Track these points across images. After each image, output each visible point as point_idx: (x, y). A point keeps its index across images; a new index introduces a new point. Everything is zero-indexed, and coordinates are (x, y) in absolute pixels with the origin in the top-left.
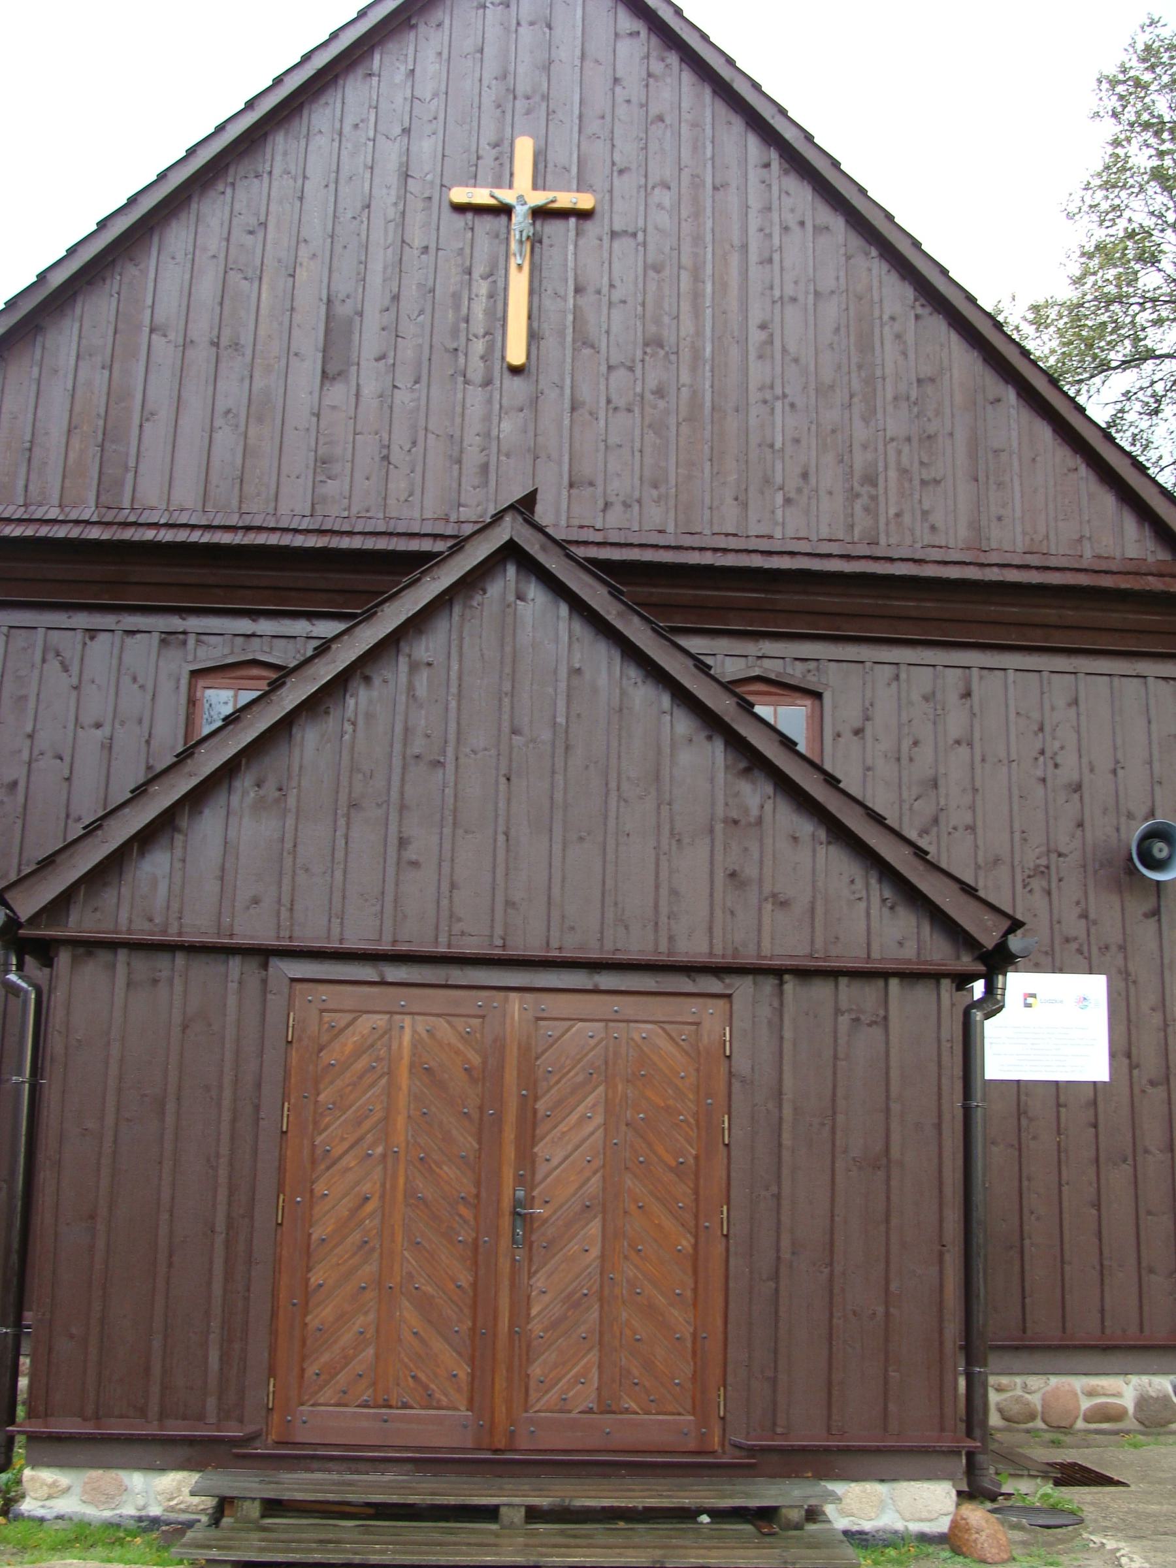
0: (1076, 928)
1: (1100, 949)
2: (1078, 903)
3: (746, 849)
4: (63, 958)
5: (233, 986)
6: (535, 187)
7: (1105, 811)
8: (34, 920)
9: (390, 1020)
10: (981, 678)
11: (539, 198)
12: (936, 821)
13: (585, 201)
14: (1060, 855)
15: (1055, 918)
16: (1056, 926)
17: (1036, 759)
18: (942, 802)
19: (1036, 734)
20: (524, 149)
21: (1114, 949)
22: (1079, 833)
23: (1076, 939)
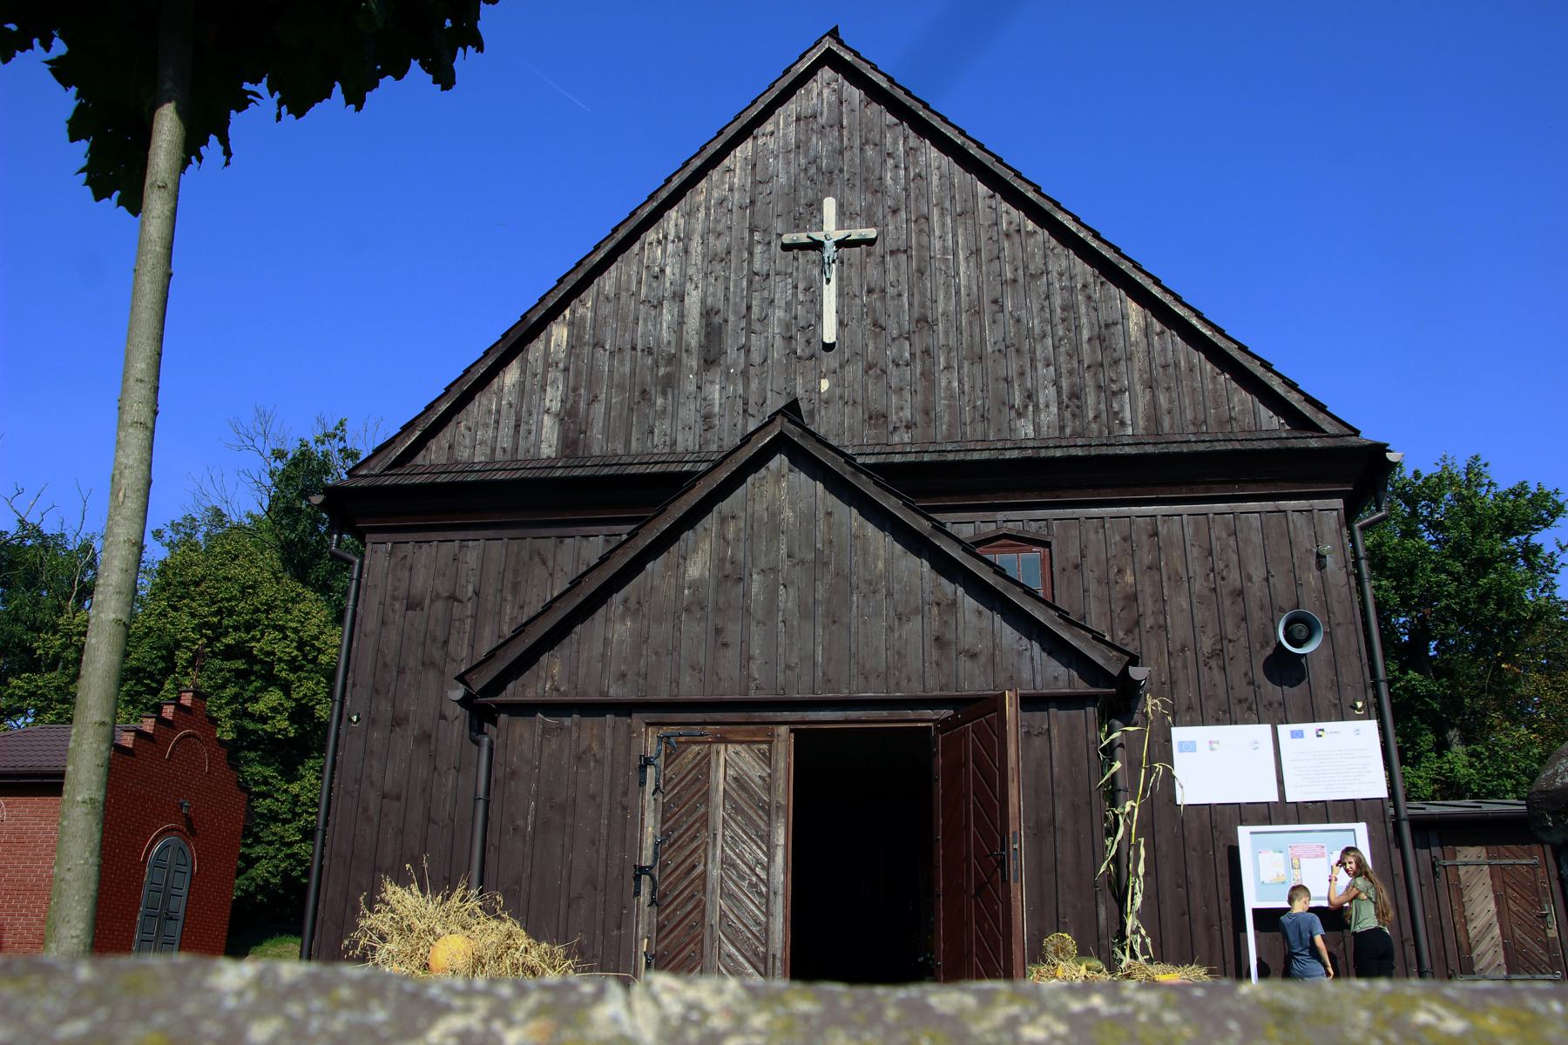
0: (1247, 692)
1: (1265, 706)
2: (1246, 674)
3: (946, 622)
4: (503, 718)
5: (608, 731)
6: (838, 229)
7: (1262, 608)
8: (485, 691)
9: (709, 747)
10: (1164, 522)
11: (841, 235)
12: (1137, 623)
13: (871, 233)
14: (1230, 641)
15: (1229, 684)
16: (1230, 692)
17: (1208, 575)
18: (1141, 609)
19: (1207, 557)
20: (830, 205)
21: (1276, 705)
22: (1243, 625)
23: (1246, 699)
